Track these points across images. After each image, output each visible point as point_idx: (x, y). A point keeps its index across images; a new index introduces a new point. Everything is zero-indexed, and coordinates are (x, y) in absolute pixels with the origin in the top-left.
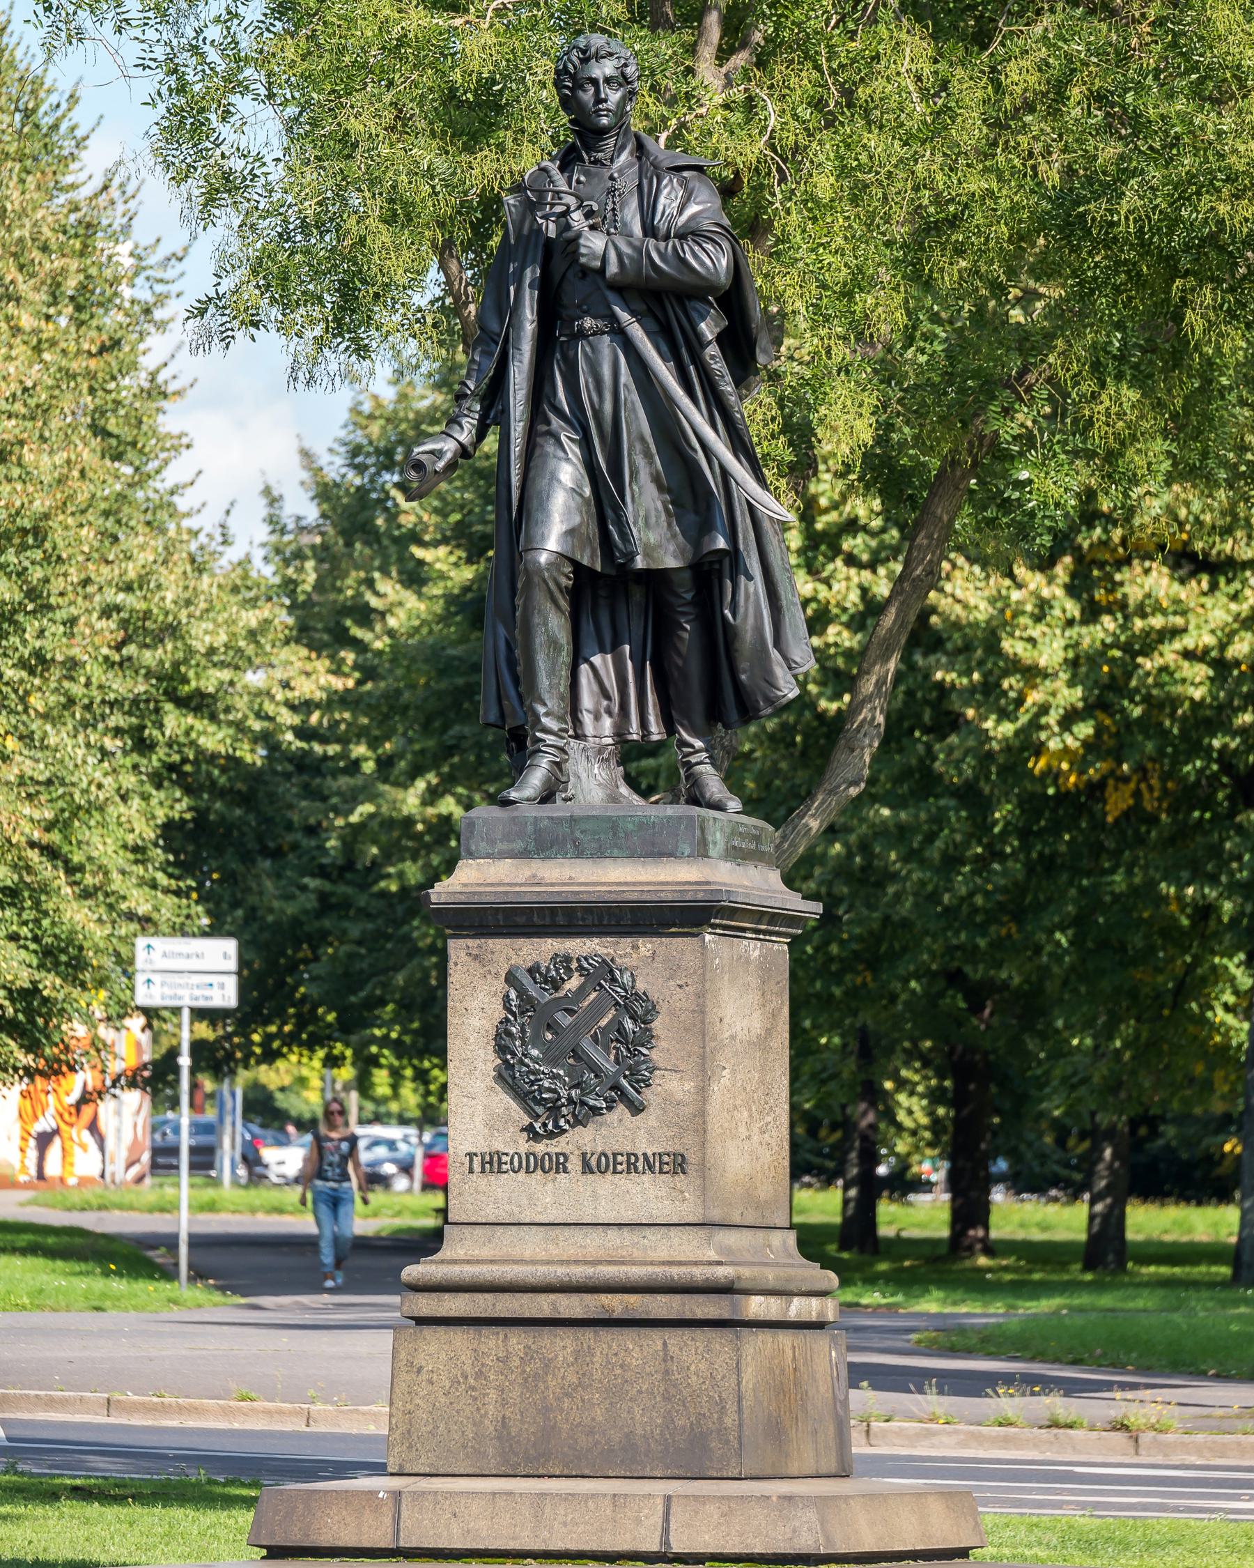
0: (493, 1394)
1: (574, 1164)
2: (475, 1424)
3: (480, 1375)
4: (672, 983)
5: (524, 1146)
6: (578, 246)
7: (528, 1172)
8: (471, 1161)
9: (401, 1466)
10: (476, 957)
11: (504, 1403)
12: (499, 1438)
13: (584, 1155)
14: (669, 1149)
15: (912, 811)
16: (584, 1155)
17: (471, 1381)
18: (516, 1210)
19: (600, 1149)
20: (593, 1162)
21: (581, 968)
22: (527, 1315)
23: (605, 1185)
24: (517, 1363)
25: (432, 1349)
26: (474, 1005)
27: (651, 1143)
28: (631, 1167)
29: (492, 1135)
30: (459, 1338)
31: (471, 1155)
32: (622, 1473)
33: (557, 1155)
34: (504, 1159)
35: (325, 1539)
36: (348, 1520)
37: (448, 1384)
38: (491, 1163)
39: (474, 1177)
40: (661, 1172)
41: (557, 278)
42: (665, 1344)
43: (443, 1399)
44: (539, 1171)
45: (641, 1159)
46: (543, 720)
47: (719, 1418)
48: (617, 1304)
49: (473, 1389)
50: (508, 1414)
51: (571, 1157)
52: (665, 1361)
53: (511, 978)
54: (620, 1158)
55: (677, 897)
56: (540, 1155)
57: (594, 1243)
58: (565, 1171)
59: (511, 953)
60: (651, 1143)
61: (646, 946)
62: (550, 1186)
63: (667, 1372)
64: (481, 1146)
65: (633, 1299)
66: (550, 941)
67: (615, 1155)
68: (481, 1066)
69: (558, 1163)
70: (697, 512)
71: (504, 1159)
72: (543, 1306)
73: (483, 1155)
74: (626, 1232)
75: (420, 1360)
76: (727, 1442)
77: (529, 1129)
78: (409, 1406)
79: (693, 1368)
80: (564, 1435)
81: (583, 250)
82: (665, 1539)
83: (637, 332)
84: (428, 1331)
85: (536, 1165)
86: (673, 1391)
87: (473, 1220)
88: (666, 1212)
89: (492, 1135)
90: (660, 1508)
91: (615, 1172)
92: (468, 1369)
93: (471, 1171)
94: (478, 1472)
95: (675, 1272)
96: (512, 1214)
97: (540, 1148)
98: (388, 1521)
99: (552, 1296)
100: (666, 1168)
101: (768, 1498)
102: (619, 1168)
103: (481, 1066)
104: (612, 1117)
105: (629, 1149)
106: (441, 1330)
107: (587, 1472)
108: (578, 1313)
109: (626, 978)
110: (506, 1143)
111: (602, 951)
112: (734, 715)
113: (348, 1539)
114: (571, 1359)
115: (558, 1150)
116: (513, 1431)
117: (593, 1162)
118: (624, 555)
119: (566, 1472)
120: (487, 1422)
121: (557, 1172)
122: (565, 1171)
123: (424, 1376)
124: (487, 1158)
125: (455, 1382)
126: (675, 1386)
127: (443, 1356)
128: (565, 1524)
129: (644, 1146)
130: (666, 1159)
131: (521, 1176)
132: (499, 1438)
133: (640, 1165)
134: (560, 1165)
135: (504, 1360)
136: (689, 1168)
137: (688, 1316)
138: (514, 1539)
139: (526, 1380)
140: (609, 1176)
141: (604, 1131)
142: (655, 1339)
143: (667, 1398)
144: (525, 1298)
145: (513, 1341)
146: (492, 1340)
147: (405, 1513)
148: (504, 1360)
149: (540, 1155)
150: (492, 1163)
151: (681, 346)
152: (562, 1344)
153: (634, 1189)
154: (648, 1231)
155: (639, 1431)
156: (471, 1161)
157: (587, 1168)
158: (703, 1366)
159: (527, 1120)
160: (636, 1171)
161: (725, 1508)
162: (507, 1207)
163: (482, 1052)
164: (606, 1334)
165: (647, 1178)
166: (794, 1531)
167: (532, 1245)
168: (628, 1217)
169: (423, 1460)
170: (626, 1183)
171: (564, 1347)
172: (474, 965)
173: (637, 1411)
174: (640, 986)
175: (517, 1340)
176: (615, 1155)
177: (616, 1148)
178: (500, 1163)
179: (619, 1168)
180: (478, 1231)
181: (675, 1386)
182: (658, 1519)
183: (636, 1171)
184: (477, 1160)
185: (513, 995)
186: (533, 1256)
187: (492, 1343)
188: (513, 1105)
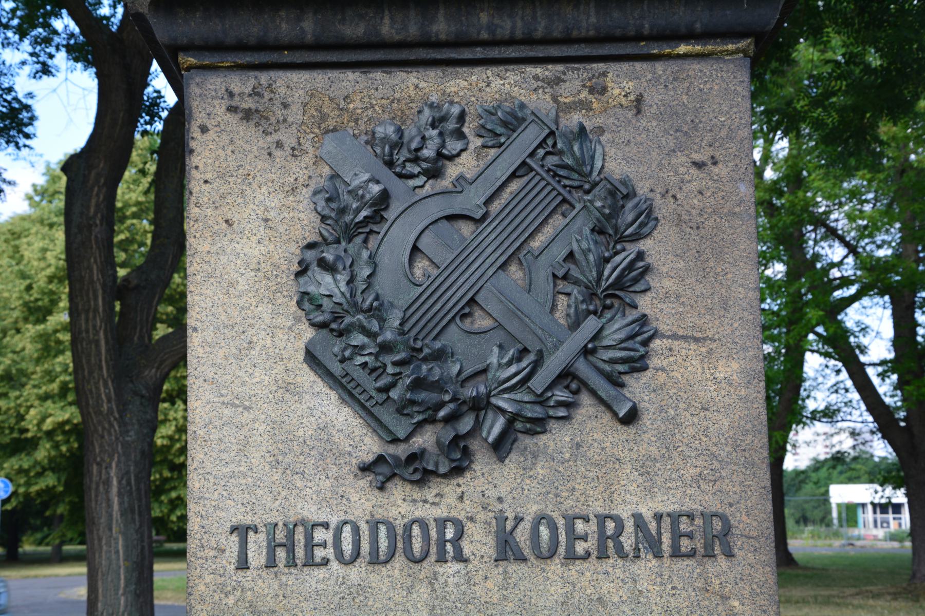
1: (479, 542)
4: (681, 158)
5: (362, 501)
8: (244, 544)
10: (247, 115)
15: (762, 145)
16: (501, 519)
19: (533, 509)
20: (522, 535)
26: (246, 214)
28: (608, 546)
31: (242, 531)
32: (401, 209)
33: (442, 523)
38: (290, 547)
40: (676, 554)
44: (399, 561)
45: (629, 527)
51: (469, 527)
54: (580, 526)
56: (399, 523)
58: (460, 558)
60: (649, 491)
61: (622, 80)
64: (269, 509)
68: (263, 339)
69: (442, 542)
71: (320, 535)
74: (230, 40)
85: (395, 546)
91: (571, 557)
93: (243, 564)
97: (400, 503)
102: (580, 547)
103: (263, 339)
104: (558, 438)
105: (598, 507)
110: (323, 502)
115: (440, 512)
121: (442, 559)
122: (460, 558)
124: (280, 536)
129: (635, 501)
130: (684, 526)
131: (356, 573)
133: (627, 540)
134: (446, 544)
136: (737, 543)
140: (555, 566)
156: (244, 544)
157: (507, 549)
160: (621, 554)
165: (647, 565)
172: (245, 132)
176: (571, 521)
178: (310, 546)
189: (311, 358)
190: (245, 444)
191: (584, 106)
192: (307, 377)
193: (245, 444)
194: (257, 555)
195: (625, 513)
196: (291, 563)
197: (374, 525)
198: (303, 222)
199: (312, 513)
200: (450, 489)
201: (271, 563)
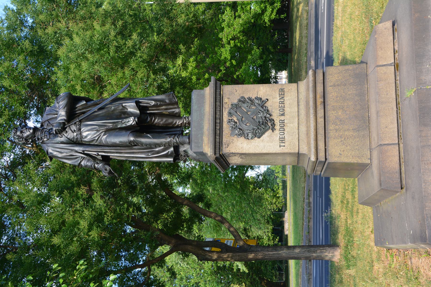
0: (346, 133)
1: (282, 118)
2: (355, 138)
3: (341, 137)
4: (235, 93)
5: (277, 132)
7: (284, 130)
9: (368, 159)
10: (228, 146)
11: (348, 130)
12: (358, 131)
13: (280, 115)
16: (280, 115)
17: (343, 139)
20: (282, 113)
23: (287, 110)
24: (337, 126)
27: (276, 98)
28: (283, 103)
30: (331, 143)
31: (280, 146)
33: (280, 122)
36: (390, 159)
37: (344, 146)
40: (284, 95)
43: (348, 147)
44: (284, 127)
45: (280, 100)
48: (320, 100)
49: (345, 139)
50: (352, 129)
52: (335, 86)
58: (284, 120)
60: (276, 98)
61: (225, 100)
62: (288, 125)
63: (338, 85)
64: (277, 143)
65: (318, 96)
68: (256, 144)
71: (281, 137)
72: (321, 121)
73: (280, 143)
76: (357, 68)
78: (351, 157)
80: (357, 113)
82: (390, 65)
85: (282, 128)
86: (343, 83)
88: (294, 93)
91: (284, 107)
92: (339, 140)
93: (284, 146)
97: (277, 127)
99: (318, 118)
103: (256, 144)
105: (278, 104)
107: (367, 106)
114: (335, 112)
116: (356, 127)
120: (354, 135)
121: (284, 122)
122: (284, 120)
123: (342, 153)
124: (281, 142)
125: (343, 144)
126: (342, 83)
127: (336, 148)
128: (387, 94)
129: (277, 100)
131: (286, 132)
132: (358, 131)
133: (282, 100)
134: (282, 122)
135: (337, 130)
136: (283, 88)
138: (393, 109)
139: (342, 124)
141: (274, 110)
142: (329, 89)
143: (345, 85)
144: (319, 126)
145: (331, 128)
146: (331, 133)
147: (387, 142)
148: (337, 130)
150: (282, 140)
152: (331, 115)
154: (300, 98)
155: (355, 92)
157: (283, 115)
158: (336, 76)
167: (303, 129)
170: (287, 103)
171: (332, 113)
172: (230, 146)
173: (349, 93)
175: (331, 127)
176: (280, 107)
177: (278, 107)
178: (282, 138)
179: (283, 137)
180: (300, 144)
181: (342, 83)
184: (282, 144)
187: (331, 134)
192: (261, 138)
194: (283, 144)
195: (279, 101)
196: (284, 140)
197: (280, 130)
198: (242, 139)
201: (284, 143)
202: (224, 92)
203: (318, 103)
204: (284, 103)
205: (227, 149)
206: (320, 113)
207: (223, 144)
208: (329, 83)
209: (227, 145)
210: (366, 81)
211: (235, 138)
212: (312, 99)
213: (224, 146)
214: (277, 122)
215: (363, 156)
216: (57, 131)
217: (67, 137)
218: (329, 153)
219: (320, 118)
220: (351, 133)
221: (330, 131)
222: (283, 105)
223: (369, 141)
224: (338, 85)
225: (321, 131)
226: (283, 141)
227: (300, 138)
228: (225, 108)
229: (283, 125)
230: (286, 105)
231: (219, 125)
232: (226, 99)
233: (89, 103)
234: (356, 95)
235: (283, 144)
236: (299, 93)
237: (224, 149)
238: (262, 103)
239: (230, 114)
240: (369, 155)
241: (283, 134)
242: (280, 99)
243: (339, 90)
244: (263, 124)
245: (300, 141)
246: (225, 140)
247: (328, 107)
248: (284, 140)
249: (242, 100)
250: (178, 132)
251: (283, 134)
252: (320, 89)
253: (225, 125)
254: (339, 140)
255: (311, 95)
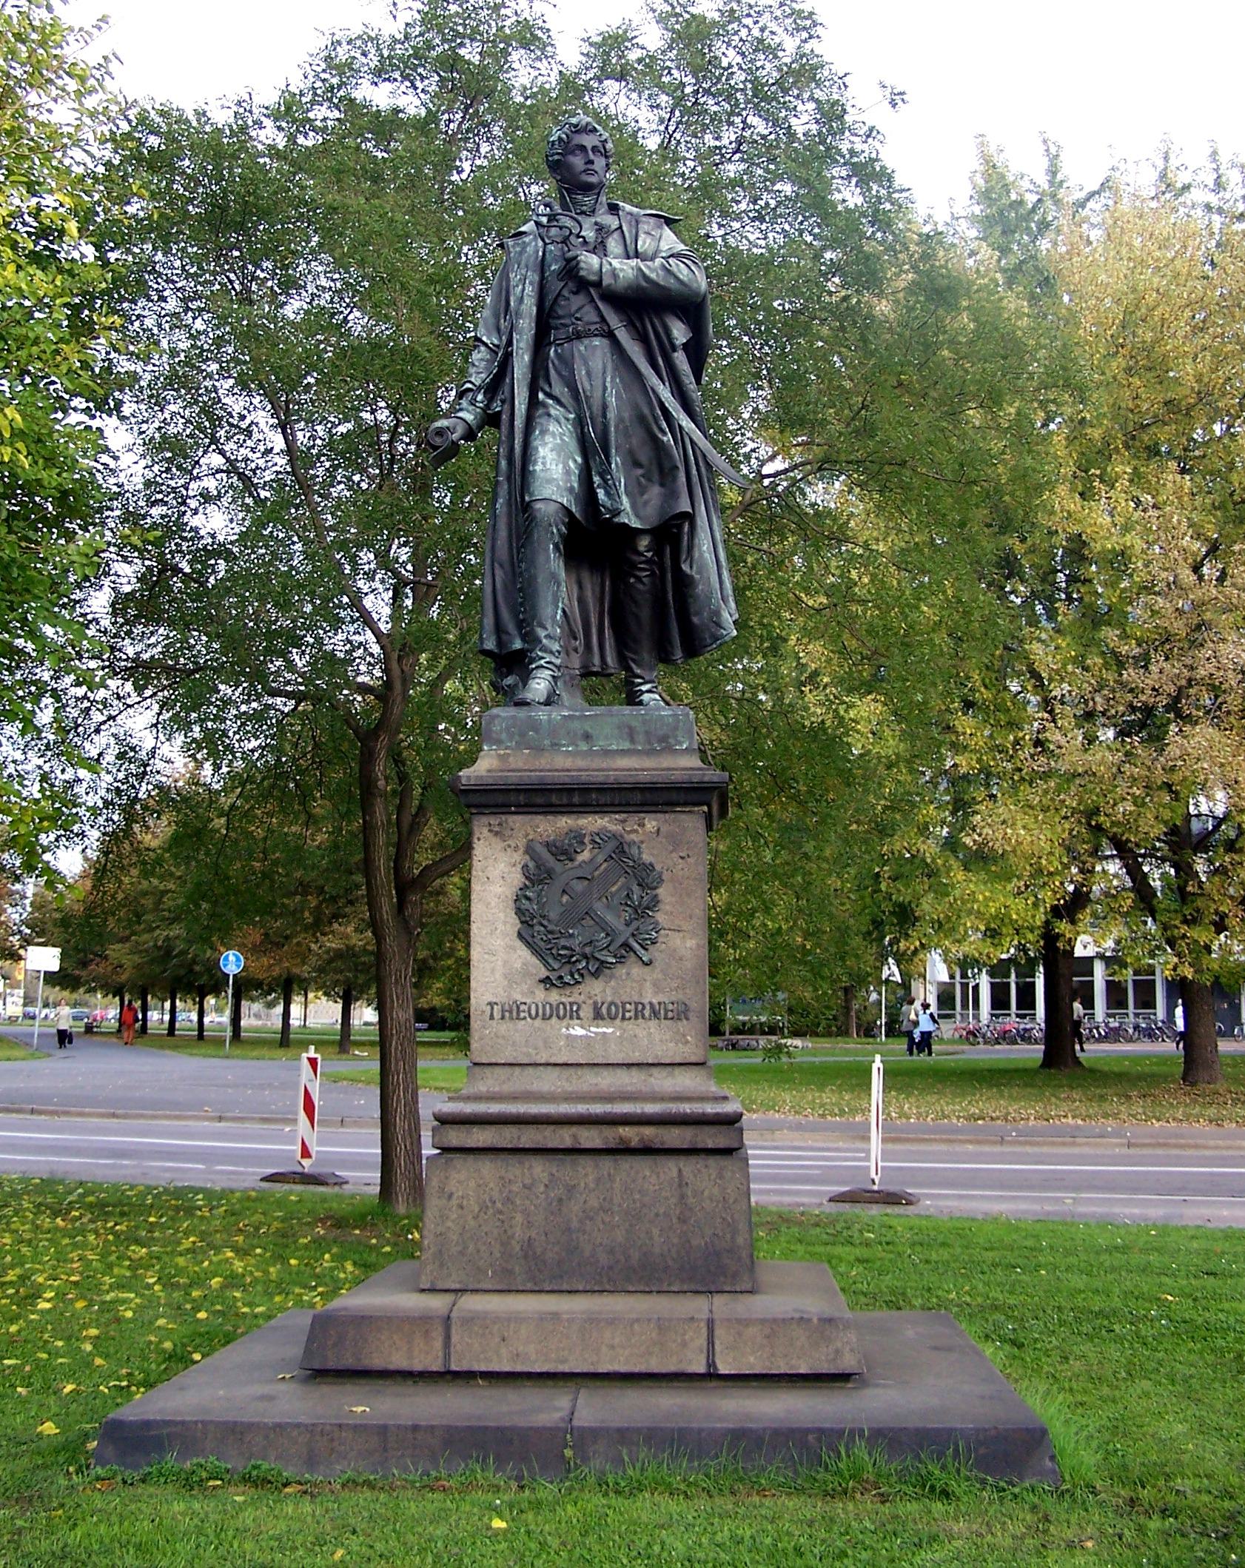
0: (519, 1218)
1: (586, 1012)
2: (502, 1244)
4: (674, 855)
5: (540, 994)
6: (578, 263)
10: (497, 834)
11: (530, 1224)
14: (673, 999)
16: (595, 1003)
17: (499, 1205)
18: (532, 1052)
19: (609, 999)
20: (604, 1010)
21: (593, 841)
22: (550, 1146)
24: (542, 1188)
25: (462, 1176)
27: (656, 993)
28: (638, 1014)
29: (511, 987)
30: (488, 1168)
31: (491, 1004)
33: (571, 1004)
34: (522, 1007)
35: (377, 1362)
38: (511, 1012)
39: (494, 1023)
41: (551, 297)
42: (680, 1170)
43: (472, 1223)
46: (544, 641)
47: (732, 1238)
48: (631, 1134)
49: (501, 1212)
50: (533, 1235)
52: (680, 1186)
53: (529, 850)
55: (686, 778)
56: (554, 1004)
57: (606, 1081)
59: (530, 830)
60: (656, 993)
61: (651, 823)
63: (682, 1197)
64: (501, 996)
65: (648, 1131)
66: (564, 819)
67: (624, 1004)
70: (662, 485)
71: (522, 1007)
72: (564, 1137)
74: (634, 1071)
75: (452, 1186)
76: (740, 1259)
77: (546, 980)
79: (706, 1193)
81: (582, 265)
83: (622, 335)
84: (458, 1160)
87: (493, 1061)
88: (671, 1053)
89: (511, 987)
90: (704, 1331)
91: (623, 1018)
92: (496, 1194)
93: (492, 1017)
94: (506, 1288)
95: (687, 1108)
96: (529, 1055)
97: (554, 996)
98: (438, 1344)
99: (574, 1129)
100: (670, 1015)
101: (809, 1320)
104: (621, 971)
105: (636, 999)
106: (471, 1158)
107: (608, 1287)
108: (598, 1143)
109: (635, 851)
110: (523, 994)
111: (612, 827)
112: (678, 654)
113: (398, 1361)
114: (592, 1185)
115: (571, 1000)
116: (539, 1251)
117: (604, 1010)
118: (609, 511)
119: (588, 1288)
120: (513, 1242)
121: (571, 1018)
122: (578, 1018)
123: (454, 1202)
124: (507, 1007)
125: (483, 1208)
126: (691, 1209)
127: (472, 1184)
128: (612, 1347)
129: (650, 997)
131: (538, 1022)
132: (526, 1257)
133: (647, 1013)
134: (573, 1013)
136: (691, 1015)
137: (700, 1146)
142: (670, 1167)
146: (518, 1171)
147: (455, 1338)
149: (554, 1004)
150: (512, 1012)
151: (659, 351)
152: (587, 1171)
153: (641, 1033)
154: (655, 1071)
158: (716, 1191)
159: (544, 973)
160: (643, 1017)
161: (767, 1331)
162: (525, 1050)
163: (502, 915)
164: (627, 1163)
165: (653, 1024)
166: (837, 1351)
167: (548, 1082)
168: (636, 1057)
169: (454, 1277)
171: (586, 1175)
172: (494, 840)
173: (656, 1232)
174: (646, 858)
175: (539, 1169)
179: (522, 1015)
180: (498, 1070)
182: (702, 1341)
183: (643, 1017)
185: (531, 865)
186: (550, 1092)
188: (535, 960)
189: (520, 936)
190: (493, 970)
191: (636, 831)
192: (519, 943)
193: (493, 970)
194: (497, 1015)
195: (646, 1001)
196: (511, 1018)
197: (544, 1007)
198: (517, 879)
199: (520, 998)
200: (576, 990)
201: (503, 1018)
202: (683, 816)
203: (625, 1131)
204: (636, 1018)
205: (485, 831)
206: (590, 1137)
207: (503, 817)
208: (689, 1166)
209: (497, 829)
210: (693, 1287)
211: (519, 857)
212: (639, 1111)
213: (494, 820)
214: (575, 995)
215: (442, 1265)
216: (574, 263)
217: (559, 294)
218: (455, 1162)
219: (574, 1136)
220: (518, 1231)
221: (527, 1165)
222: (632, 1014)
223: (490, 1287)
224: (682, 1197)
225: (529, 1137)
226: (507, 1014)
227: (517, 1070)
228: (624, 821)
229: (562, 1012)
230: (629, 1025)
231: (565, 801)
232: (654, 823)
233: (680, 359)
234: (645, 1254)
235: (497, 1015)
236: (669, 1069)
237: (484, 820)
238: (630, 947)
239: (599, 840)
240: (446, 1287)
241: (533, 1012)
242: (651, 1004)
243: (667, 1198)
244: (571, 947)
245: (508, 1070)
246: (516, 821)
247: (607, 1163)
248: (511, 1018)
249: (645, 877)
250: (597, 660)
251: (533, 1012)
252: (674, 1137)
253: (565, 822)
254: (496, 1194)
255: (651, 1108)
